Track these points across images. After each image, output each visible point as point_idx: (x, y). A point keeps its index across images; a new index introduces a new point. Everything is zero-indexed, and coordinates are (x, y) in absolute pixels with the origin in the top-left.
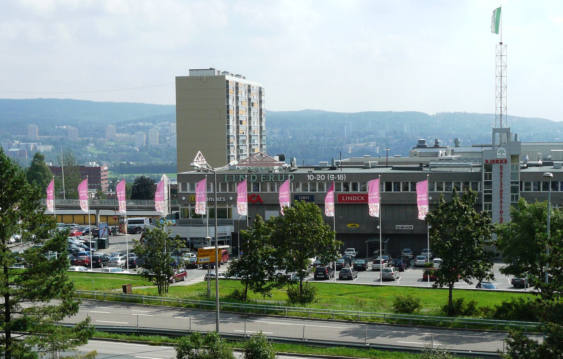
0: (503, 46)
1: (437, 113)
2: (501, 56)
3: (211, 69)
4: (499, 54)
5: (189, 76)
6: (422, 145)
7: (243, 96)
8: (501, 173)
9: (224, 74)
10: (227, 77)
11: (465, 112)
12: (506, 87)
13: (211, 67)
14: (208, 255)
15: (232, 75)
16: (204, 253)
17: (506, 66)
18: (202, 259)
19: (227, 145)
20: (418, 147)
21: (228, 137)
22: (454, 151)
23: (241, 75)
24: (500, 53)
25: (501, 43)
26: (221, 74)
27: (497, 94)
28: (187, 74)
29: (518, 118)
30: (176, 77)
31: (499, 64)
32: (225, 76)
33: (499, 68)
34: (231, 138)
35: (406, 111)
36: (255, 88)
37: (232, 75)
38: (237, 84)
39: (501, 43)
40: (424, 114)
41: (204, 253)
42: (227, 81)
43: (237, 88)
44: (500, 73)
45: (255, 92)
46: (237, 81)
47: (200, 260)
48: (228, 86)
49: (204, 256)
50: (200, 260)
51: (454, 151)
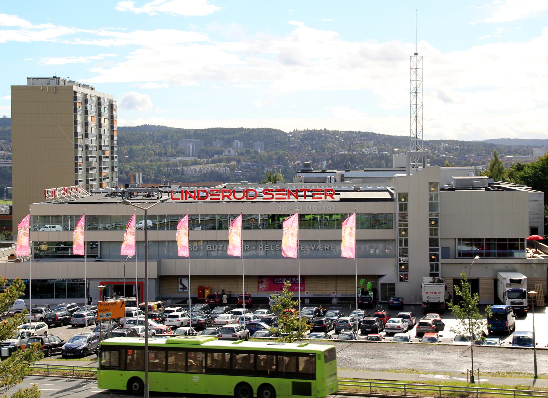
0: (418, 58)
1: (294, 130)
2: (416, 69)
3: (55, 77)
4: (414, 67)
5: (27, 85)
6: (306, 169)
7: (92, 110)
8: (430, 205)
9: (70, 84)
10: (75, 88)
11: (325, 129)
12: (422, 105)
13: (55, 76)
14: (109, 310)
15: (79, 85)
16: (106, 307)
17: (422, 80)
18: (102, 315)
19: (74, 168)
20: (303, 171)
21: (76, 158)
22: (345, 176)
23: (88, 86)
24: (415, 65)
25: (416, 54)
26: (66, 84)
27: (412, 112)
28: (25, 83)
29: (383, 135)
30: (11, 86)
31: (414, 78)
32: (72, 86)
33: (414, 83)
34: (80, 160)
35: (259, 128)
36: (106, 100)
37: (79, 85)
38: (86, 95)
39: (416, 54)
40: (279, 131)
41: (106, 307)
42: (75, 93)
43: (86, 101)
44: (415, 89)
45: (105, 104)
46: (86, 92)
47: (101, 316)
48: (75, 98)
49: (105, 310)
50: (101, 316)
51: (345, 176)
